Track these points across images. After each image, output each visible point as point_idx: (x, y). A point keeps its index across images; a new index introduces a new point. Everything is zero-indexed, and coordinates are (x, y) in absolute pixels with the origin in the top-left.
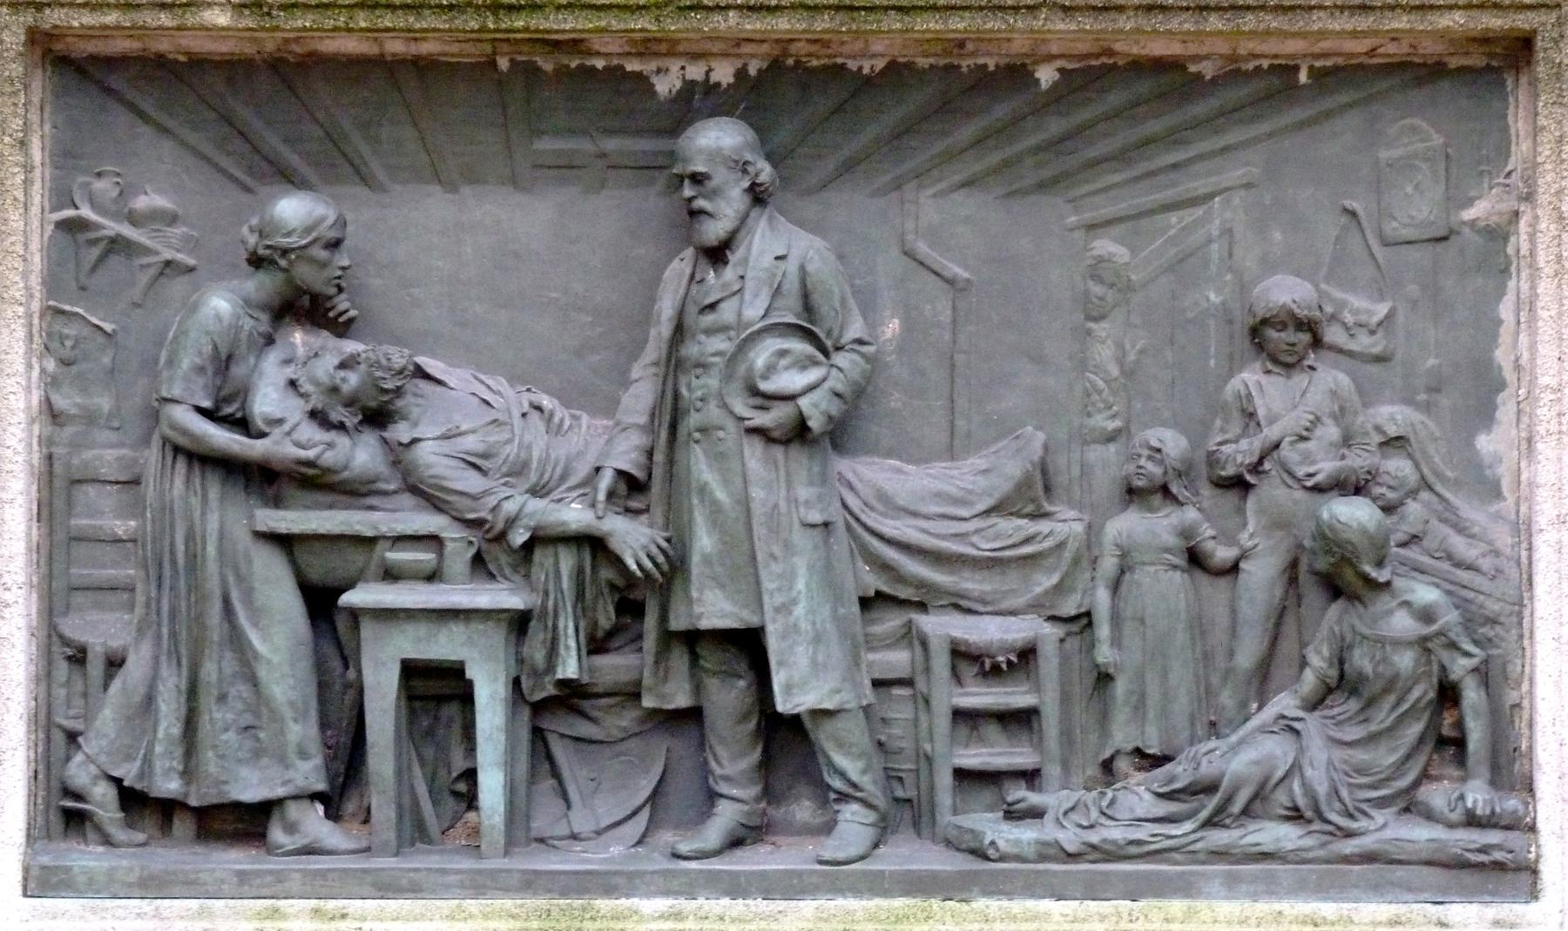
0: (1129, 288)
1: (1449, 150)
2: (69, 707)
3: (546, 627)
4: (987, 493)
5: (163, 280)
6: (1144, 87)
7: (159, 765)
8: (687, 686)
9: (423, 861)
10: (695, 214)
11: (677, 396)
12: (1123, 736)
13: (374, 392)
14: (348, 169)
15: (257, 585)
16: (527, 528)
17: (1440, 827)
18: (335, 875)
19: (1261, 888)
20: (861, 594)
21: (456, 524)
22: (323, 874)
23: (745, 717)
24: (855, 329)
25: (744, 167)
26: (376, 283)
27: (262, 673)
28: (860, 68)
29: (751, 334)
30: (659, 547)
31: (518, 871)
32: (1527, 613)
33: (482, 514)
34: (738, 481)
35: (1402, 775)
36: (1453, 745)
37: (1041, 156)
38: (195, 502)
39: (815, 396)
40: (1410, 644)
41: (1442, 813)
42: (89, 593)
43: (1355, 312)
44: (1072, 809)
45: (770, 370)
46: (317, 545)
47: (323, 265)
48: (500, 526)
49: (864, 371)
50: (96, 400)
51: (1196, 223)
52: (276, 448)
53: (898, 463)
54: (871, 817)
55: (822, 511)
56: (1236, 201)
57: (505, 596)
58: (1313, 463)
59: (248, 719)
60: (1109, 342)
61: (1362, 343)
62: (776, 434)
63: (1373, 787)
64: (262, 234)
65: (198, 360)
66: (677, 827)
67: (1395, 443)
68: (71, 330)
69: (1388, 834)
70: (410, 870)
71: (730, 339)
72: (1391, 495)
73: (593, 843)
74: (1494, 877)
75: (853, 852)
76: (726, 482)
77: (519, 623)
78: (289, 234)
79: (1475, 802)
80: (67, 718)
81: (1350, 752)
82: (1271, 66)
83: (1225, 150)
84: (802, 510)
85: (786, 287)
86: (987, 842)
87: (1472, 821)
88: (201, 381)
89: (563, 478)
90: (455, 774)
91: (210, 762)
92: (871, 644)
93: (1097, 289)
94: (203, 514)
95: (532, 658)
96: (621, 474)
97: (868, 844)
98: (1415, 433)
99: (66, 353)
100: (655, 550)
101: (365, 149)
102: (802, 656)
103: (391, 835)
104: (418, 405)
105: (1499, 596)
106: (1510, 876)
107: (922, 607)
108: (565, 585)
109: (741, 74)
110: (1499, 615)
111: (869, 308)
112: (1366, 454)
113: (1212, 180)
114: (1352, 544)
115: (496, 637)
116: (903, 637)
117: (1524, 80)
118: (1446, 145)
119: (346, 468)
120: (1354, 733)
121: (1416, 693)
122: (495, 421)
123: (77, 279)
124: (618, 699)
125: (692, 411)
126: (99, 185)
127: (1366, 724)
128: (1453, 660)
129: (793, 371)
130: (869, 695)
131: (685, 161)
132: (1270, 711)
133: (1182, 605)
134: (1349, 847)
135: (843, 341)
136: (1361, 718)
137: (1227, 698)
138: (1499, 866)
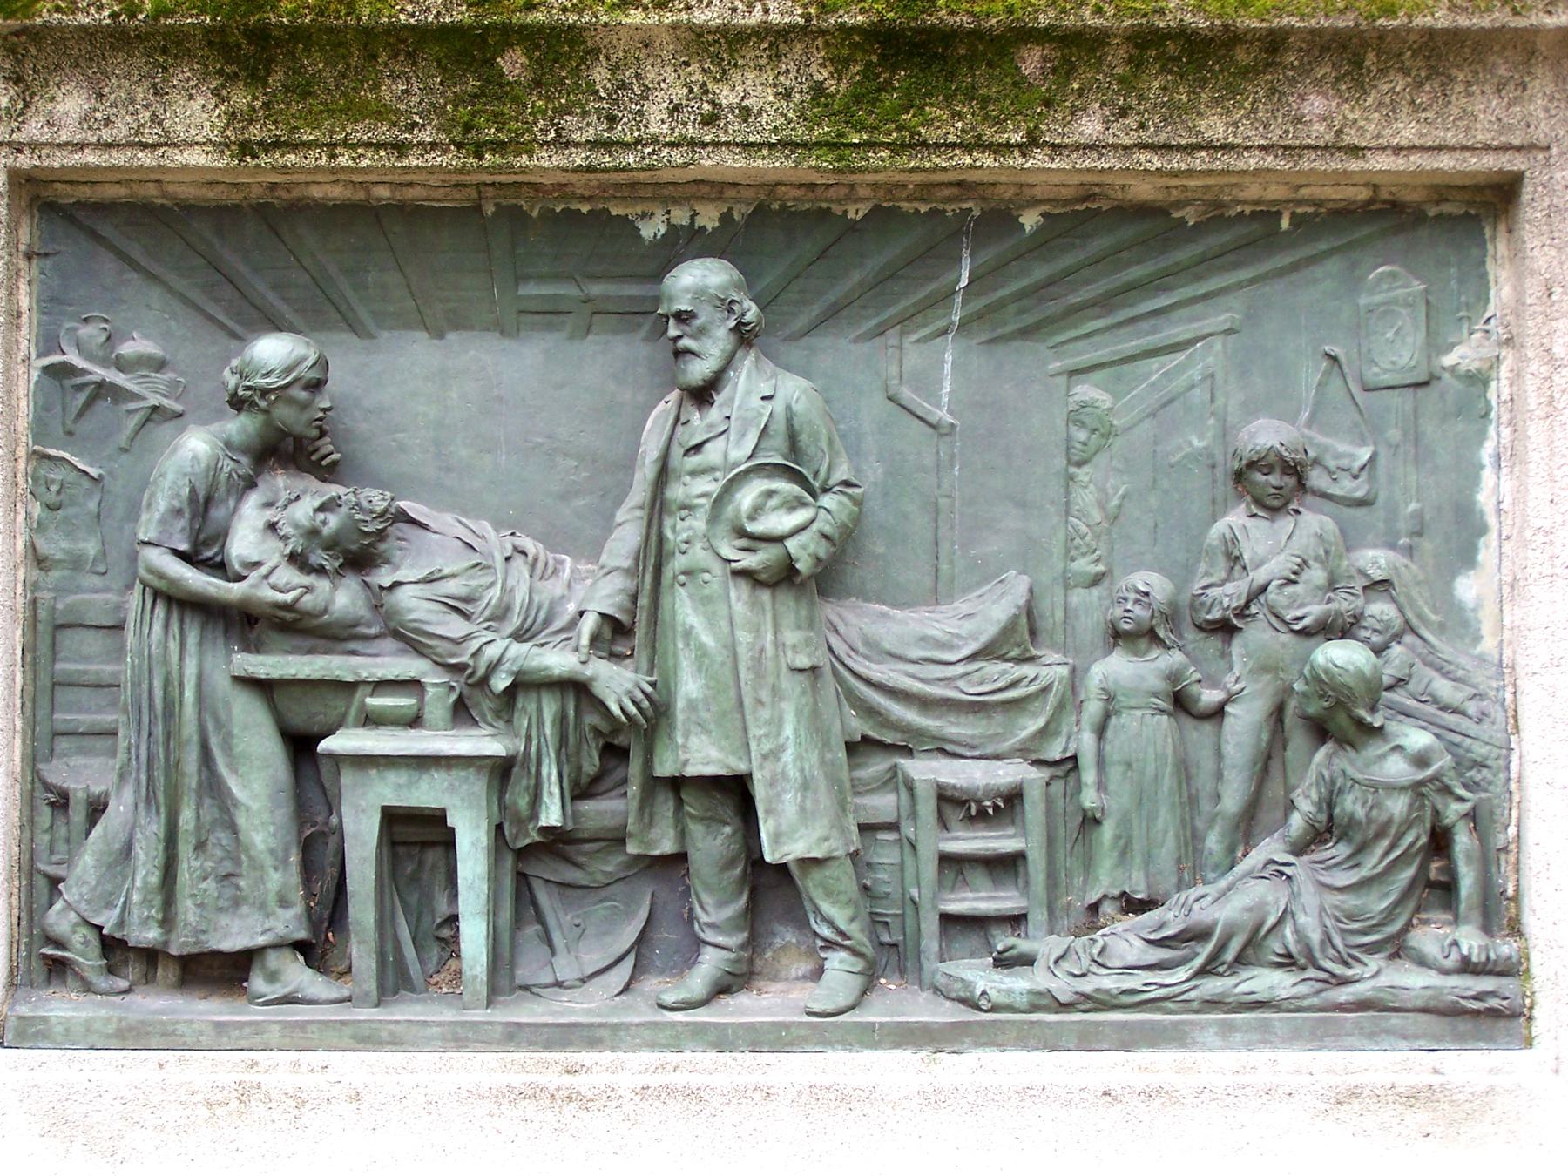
0: (1109, 434)
1: (1430, 298)
2: (52, 852)
3: (529, 772)
4: (973, 636)
5: (150, 425)
6: (1127, 232)
7: (136, 914)
8: (672, 833)
9: (404, 1012)
10: (679, 354)
11: (661, 539)
12: (1106, 881)
13: (355, 536)
14: (335, 316)
15: (236, 731)
16: (510, 673)
17: (1433, 973)
18: (314, 1027)
19: (1256, 1037)
20: (848, 738)
21: (439, 669)
22: (302, 1025)
23: (730, 864)
24: (842, 473)
25: (729, 306)
26: (364, 427)
27: (241, 821)
28: (846, 212)
29: (737, 475)
30: (643, 692)
31: (501, 1023)
32: (1514, 757)
33: (464, 659)
34: (724, 624)
35: (1393, 920)
36: (1446, 890)
37: (1025, 302)
38: (173, 646)
39: (803, 537)
40: (1403, 789)
41: (1435, 959)
42: (72, 738)
43: (1338, 456)
44: (1062, 957)
45: (756, 512)
46: (297, 692)
47: (304, 406)
48: (481, 671)
49: (851, 513)
50: (82, 545)
51: (1181, 368)
52: (253, 591)
53: (885, 608)
54: (859, 965)
55: (809, 656)
56: (1218, 346)
57: (484, 742)
58: (1302, 605)
59: (228, 867)
60: (1091, 486)
61: (1346, 487)
62: (763, 577)
63: (1364, 932)
64: (242, 375)
65: (176, 504)
66: (661, 972)
67: (1379, 587)
68: (57, 475)
69: (1384, 980)
70: (390, 1022)
71: (716, 480)
72: (1375, 639)
73: (576, 992)
74: (1485, 1024)
75: (842, 1000)
76: (711, 621)
77: (501, 771)
78: (267, 375)
79: (1470, 948)
80: (51, 863)
81: (1341, 897)
82: (1253, 212)
83: (1206, 297)
84: (789, 653)
85: (772, 427)
86: (978, 992)
87: (1467, 967)
88: (182, 523)
89: (547, 622)
90: (438, 920)
91: (187, 910)
92: (858, 788)
93: (1082, 435)
94: (181, 659)
95: (515, 804)
96: (603, 615)
97: (857, 993)
98: (1399, 576)
99: (52, 498)
100: (639, 696)
101: (350, 295)
102: (790, 803)
103: (371, 986)
104: (401, 549)
105: (1487, 740)
106: (1502, 1024)
107: (907, 751)
108: (548, 731)
109: (726, 218)
110: (1486, 759)
111: (855, 453)
112: (1352, 598)
113: (1195, 325)
114: (1349, 688)
115: (477, 785)
116: (885, 783)
117: (1502, 228)
118: (1426, 291)
119: (325, 611)
120: (1344, 878)
121: (1409, 839)
122: (479, 564)
123: (64, 424)
124: (603, 844)
125: (677, 554)
126: (85, 331)
127: (1356, 870)
128: (1446, 806)
129: (782, 512)
130: (855, 841)
131: (671, 299)
132: (1257, 857)
133: (1169, 750)
134: (1344, 994)
135: (831, 482)
136: (1351, 864)
137: (1213, 842)
138: (1494, 1013)
